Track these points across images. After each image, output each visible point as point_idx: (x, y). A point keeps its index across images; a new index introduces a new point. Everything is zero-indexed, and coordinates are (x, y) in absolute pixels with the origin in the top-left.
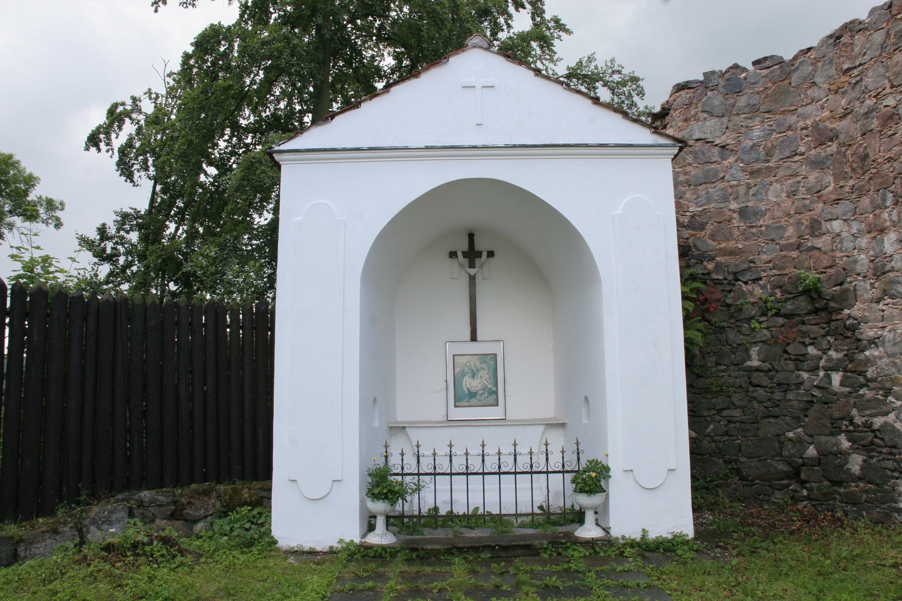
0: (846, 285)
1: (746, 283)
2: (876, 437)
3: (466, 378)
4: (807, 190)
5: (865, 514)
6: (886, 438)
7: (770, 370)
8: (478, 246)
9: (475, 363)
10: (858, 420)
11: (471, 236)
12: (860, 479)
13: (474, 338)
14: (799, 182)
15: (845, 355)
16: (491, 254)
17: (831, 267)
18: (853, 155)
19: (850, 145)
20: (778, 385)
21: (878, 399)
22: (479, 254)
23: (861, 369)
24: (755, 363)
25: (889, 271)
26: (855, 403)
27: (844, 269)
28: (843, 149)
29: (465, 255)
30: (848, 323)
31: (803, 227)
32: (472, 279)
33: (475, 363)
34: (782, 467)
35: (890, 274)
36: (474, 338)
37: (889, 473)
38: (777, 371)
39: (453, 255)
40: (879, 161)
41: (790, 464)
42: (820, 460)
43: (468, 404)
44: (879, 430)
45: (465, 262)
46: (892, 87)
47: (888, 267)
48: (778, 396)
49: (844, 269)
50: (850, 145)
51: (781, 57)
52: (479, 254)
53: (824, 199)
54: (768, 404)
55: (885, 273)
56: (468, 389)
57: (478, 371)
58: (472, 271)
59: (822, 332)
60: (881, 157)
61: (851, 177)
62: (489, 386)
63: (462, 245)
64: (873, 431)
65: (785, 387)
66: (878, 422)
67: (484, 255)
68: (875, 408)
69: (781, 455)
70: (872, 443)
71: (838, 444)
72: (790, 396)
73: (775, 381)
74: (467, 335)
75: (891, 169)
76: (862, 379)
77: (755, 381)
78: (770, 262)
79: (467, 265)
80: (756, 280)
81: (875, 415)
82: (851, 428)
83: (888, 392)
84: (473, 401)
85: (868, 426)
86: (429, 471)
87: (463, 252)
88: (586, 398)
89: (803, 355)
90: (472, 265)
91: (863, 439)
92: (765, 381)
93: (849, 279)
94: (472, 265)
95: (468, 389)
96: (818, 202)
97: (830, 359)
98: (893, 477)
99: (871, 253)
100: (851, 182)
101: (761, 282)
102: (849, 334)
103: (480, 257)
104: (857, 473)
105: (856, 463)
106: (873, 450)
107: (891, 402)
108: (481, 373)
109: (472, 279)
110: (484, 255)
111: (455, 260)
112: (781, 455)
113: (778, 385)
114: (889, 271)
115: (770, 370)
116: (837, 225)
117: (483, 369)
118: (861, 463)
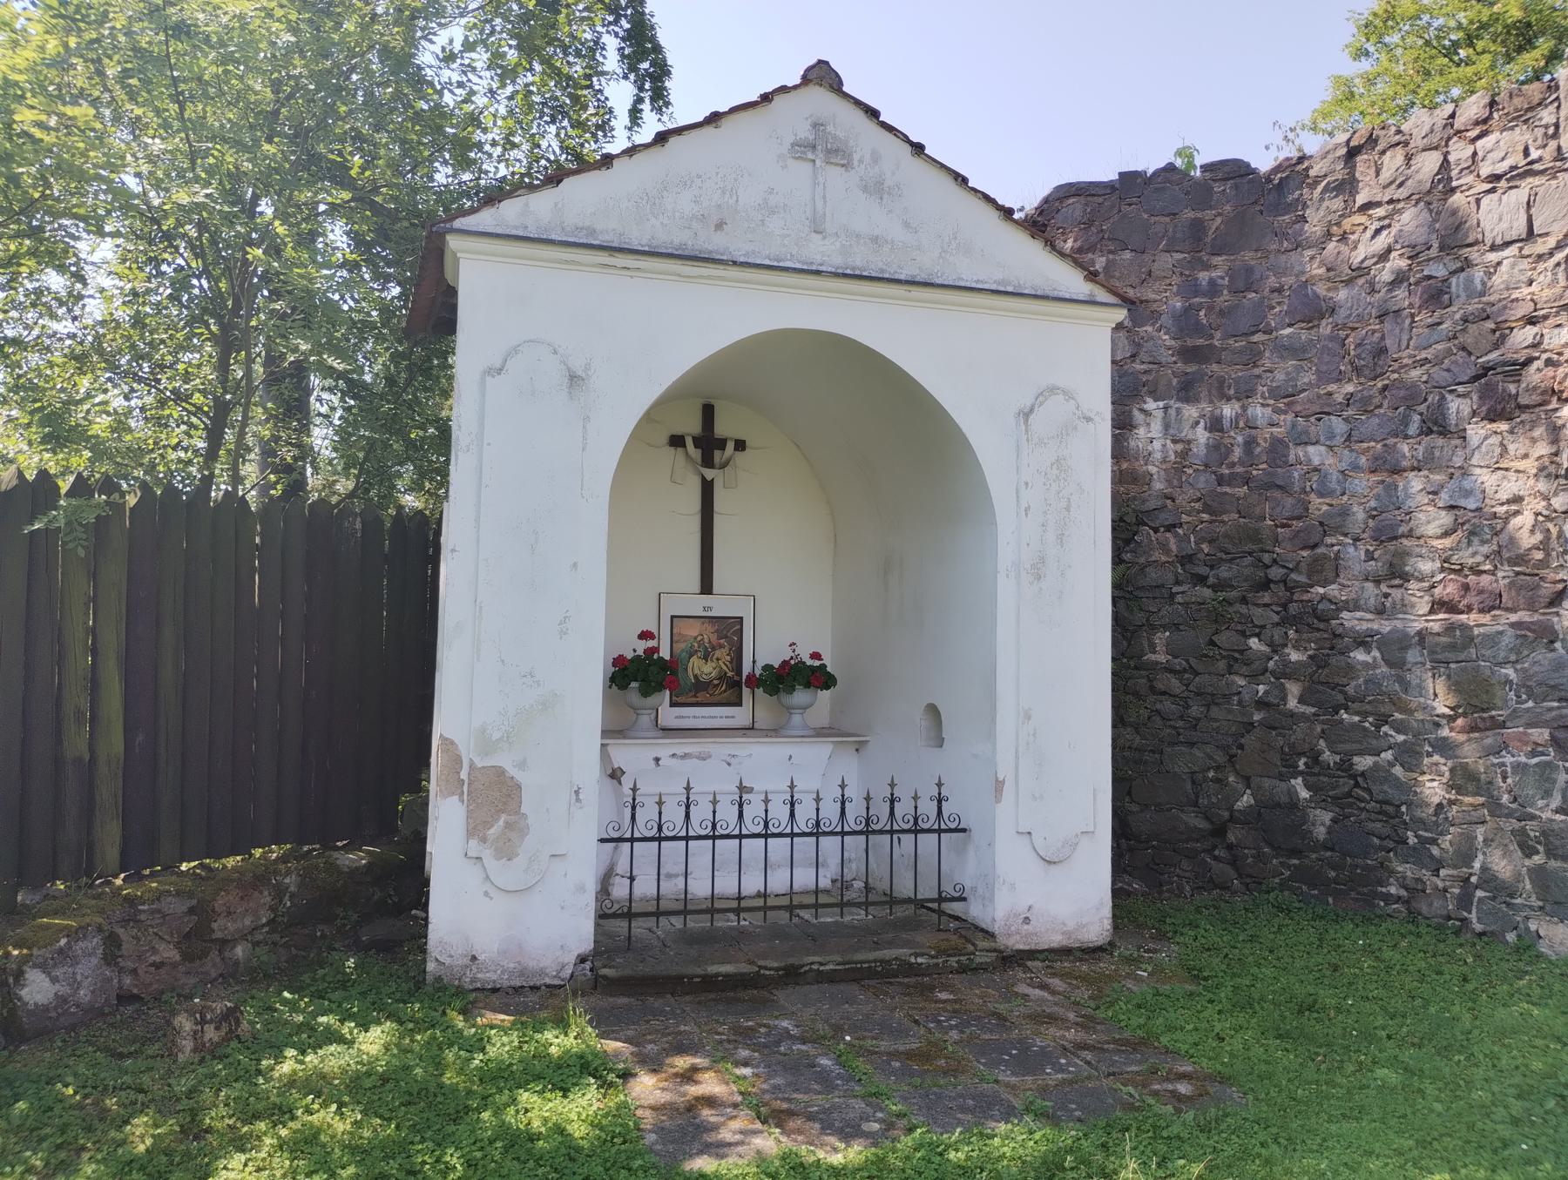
0: (1321, 550)
1: (1156, 530)
2: (1357, 785)
3: (694, 659)
4: (1270, 391)
5: (1330, 900)
6: (1375, 788)
7: (1185, 671)
8: (722, 428)
9: (709, 635)
10: (1327, 756)
11: (708, 412)
12: (1326, 847)
13: (707, 587)
14: (1259, 377)
15: (1310, 657)
16: (740, 445)
17: (1299, 518)
18: (1358, 345)
19: (1353, 329)
20: (1198, 694)
21: (1365, 729)
22: (722, 443)
23: (1337, 680)
24: (1161, 658)
25: (1403, 536)
26: (1323, 731)
27: (1321, 524)
28: (1342, 334)
29: (697, 442)
30: (1320, 607)
31: (1259, 450)
32: (707, 489)
33: (709, 635)
34: (1202, 824)
35: (1405, 541)
36: (707, 587)
37: (1376, 841)
38: (1197, 674)
39: (677, 441)
40: (1405, 361)
41: (1207, 818)
42: (1260, 814)
43: (694, 700)
44: (1363, 774)
45: (695, 453)
46: (1441, 249)
47: (1403, 529)
48: (1195, 710)
49: (1321, 524)
50: (1353, 329)
51: (1248, 165)
52: (722, 443)
53: (1298, 408)
54: (1180, 724)
55: (1396, 538)
56: (696, 677)
57: (714, 649)
58: (709, 474)
59: (1276, 618)
60: (1410, 357)
61: (1350, 380)
62: (730, 674)
63: (691, 425)
64: (1354, 777)
65: (1211, 700)
66: (1363, 763)
67: (730, 446)
68: (1360, 742)
69: (1196, 804)
70: (1349, 795)
71: (1292, 793)
72: (1215, 712)
73: (1191, 688)
74: (695, 584)
75: (1425, 378)
76: (1340, 698)
77: (1160, 686)
78: (1199, 499)
79: (699, 460)
80: (1170, 528)
81: (1361, 753)
82: (1316, 770)
83: (1383, 720)
84: (701, 697)
85: (1345, 766)
86: (703, 833)
87: (694, 439)
88: (933, 711)
89: (1241, 652)
90: (708, 462)
91: (1334, 789)
92: (1175, 684)
93: (1329, 540)
94: (708, 462)
95: (696, 677)
96: (1285, 413)
97: (1286, 663)
98: (1382, 848)
99: (1373, 504)
100: (1350, 388)
101: (1180, 531)
102: (1317, 621)
103: (723, 449)
104: (1321, 837)
105: (1321, 821)
106: (1351, 805)
107: (1386, 734)
108: (718, 653)
109: (707, 489)
110: (730, 446)
111: (680, 450)
112: (1196, 804)
113: (1198, 694)
114: (1403, 536)
115: (1185, 671)
116: (1316, 454)
117: (721, 646)
118: (1328, 823)
